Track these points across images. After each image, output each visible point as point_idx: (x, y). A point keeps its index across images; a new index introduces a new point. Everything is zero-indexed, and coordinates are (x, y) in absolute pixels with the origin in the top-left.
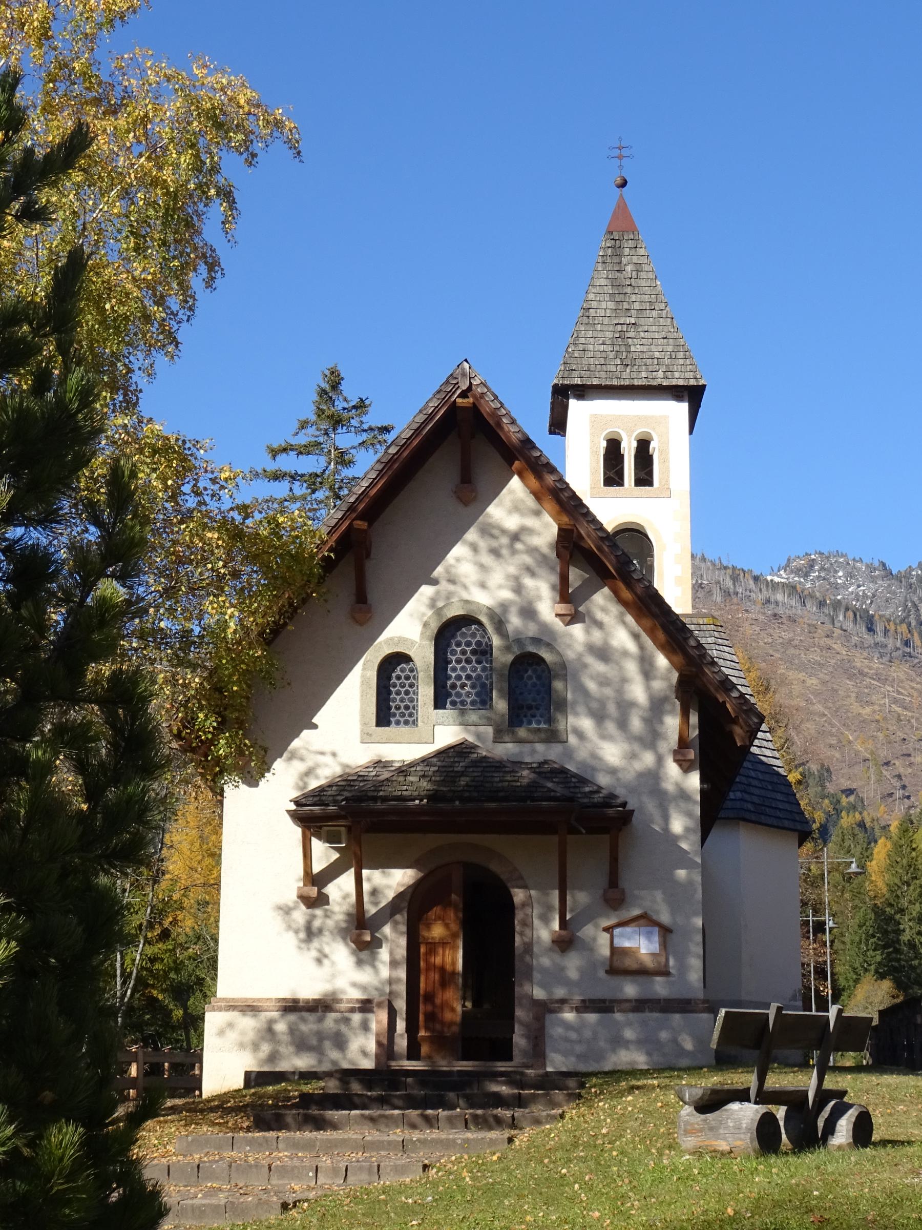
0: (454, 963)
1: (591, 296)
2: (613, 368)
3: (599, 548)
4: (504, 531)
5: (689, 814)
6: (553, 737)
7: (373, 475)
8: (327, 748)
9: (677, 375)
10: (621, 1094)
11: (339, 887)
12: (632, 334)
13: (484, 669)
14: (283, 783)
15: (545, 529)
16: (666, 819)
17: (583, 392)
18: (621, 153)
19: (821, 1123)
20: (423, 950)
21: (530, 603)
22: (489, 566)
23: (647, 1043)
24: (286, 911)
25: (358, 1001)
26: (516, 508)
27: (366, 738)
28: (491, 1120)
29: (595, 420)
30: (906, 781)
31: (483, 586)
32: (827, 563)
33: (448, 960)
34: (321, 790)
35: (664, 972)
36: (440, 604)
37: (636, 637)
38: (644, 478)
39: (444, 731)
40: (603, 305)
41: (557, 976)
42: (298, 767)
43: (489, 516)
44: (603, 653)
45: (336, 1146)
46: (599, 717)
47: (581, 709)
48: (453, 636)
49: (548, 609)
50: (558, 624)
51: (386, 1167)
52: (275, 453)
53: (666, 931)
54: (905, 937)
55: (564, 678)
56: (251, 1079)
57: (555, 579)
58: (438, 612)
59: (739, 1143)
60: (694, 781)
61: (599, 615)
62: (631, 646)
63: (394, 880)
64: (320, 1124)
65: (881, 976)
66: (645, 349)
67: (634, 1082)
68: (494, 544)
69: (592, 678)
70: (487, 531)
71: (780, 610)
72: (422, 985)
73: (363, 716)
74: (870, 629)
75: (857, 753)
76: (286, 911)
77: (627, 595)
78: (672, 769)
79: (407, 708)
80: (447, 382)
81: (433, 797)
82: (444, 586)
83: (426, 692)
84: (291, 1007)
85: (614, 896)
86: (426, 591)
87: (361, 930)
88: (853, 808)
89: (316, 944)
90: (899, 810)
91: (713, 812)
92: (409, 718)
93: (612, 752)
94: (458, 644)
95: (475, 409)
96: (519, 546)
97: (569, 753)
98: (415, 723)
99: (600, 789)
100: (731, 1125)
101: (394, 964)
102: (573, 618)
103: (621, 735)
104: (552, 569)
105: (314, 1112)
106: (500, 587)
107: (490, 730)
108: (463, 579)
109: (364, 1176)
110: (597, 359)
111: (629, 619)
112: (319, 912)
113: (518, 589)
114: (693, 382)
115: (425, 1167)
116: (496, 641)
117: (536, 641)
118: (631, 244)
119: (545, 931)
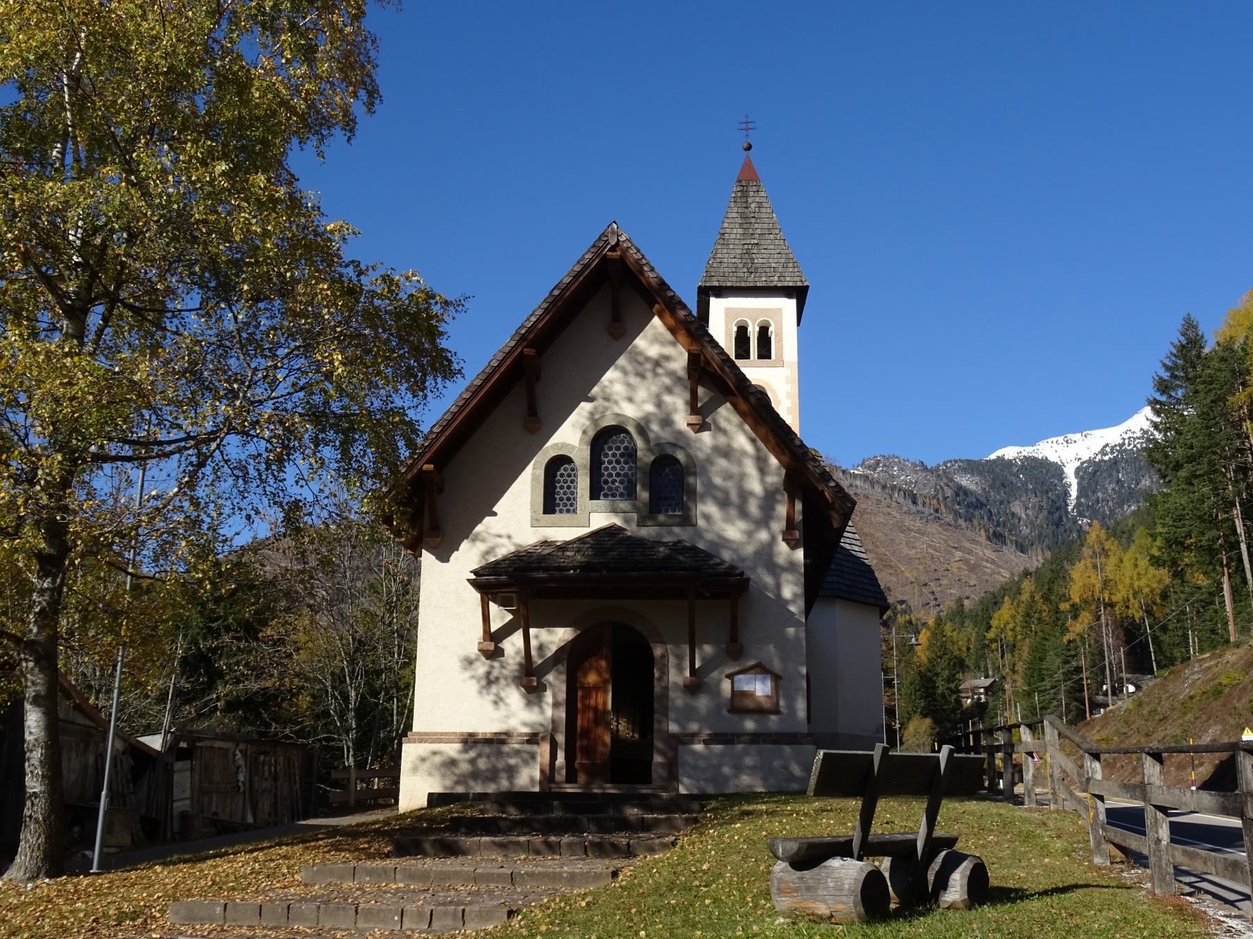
0: (605, 704)
1: (726, 225)
3: (722, 369)
4: (648, 359)
5: (796, 585)
6: (687, 521)
7: (540, 312)
8: (504, 532)
10: (732, 821)
11: (513, 644)
13: (630, 469)
14: (468, 557)
15: (679, 359)
16: (778, 587)
17: (721, 292)
18: (747, 126)
19: (931, 877)
20: (580, 693)
22: (636, 388)
23: (763, 770)
25: (526, 734)
26: (656, 340)
27: (535, 523)
28: (608, 847)
29: (728, 311)
30: (937, 595)
31: (630, 400)
32: (888, 461)
33: (600, 701)
34: (497, 563)
35: (776, 711)
36: (597, 417)
37: (753, 441)
38: (765, 353)
39: (599, 518)
41: (688, 713)
42: (481, 547)
43: (635, 347)
44: (726, 452)
45: (449, 878)
46: (724, 503)
48: (606, 442)
49: (682, 420)
50: (690, 432)
51: (471, 912)
53: (776, 678)
54: (939, 691)
55: (694, 474)
56: (434, 799)
57: (687, 395)
58: (595, 422)
59: (840, 907)
60: (800, 554)
61: (723, 424)
62: (749, 448)
63: (559, 636)
64: (452, 850)
65: (925, 716)
67: (746, 808)
71: (859, 491)
72: (579, 723)
73: (532, 505)
74: (914, 502)
75: (907, 578)
76: (469, 662)
77: (743, 406)
78: (783, 547)
79: (569, 499)
80: (600, 239)
81: (585, 567)
83: (583, 483)
84: (470, 741)
86: (585, 407)
87: (530, 678)
88: (904, 612)
89: (494, 689)
90: (933, 613)
91: (814, 590)
92: (570, 507)
93: (734, 531)
94: (610, 449)
95: (622, 260)
96: (660, 371)
97: (699, 534)
98: (575, 511)
99: (723, 562)
100: (831, 885)
101: (556, 705)
102: (701, 427)
103: (740, 521)
104: (686, 388)
105: (449, 837)
106: (644, 402)
108: (615, 397)
109: (449, 922)
110: (729, 267)
111: (747, 427)
112: (496, 664)
113: (659, 404)
114: (799, 284)
115: (511, 914)
116: (639, 443)
117: (674, 445)
118: (755, 189)
119: (677, 676)
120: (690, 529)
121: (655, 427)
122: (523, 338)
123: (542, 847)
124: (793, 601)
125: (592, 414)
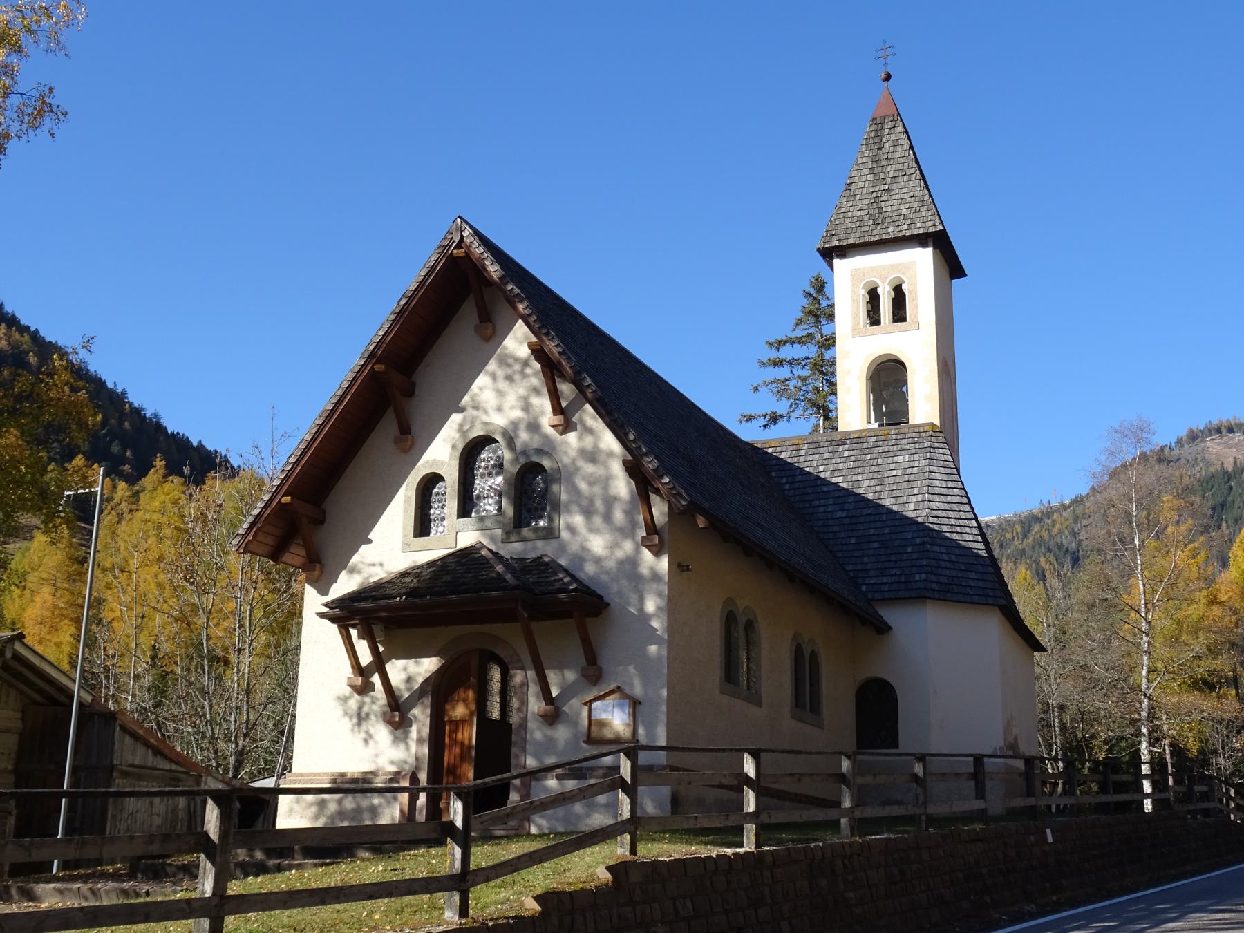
0: (470, 739)
1: (855, 173)
2: (866, 229)
4: (517, 360)
5: (660, 595)
6: (550, 534)
8: (377, 561)
9: (919, 225)
12: (885, 198)
16: (641, 600)
17: (843, 251)
20: (447, 728)
21: (536, 419)
22: (503, 394)
24: (344, 700)
31: (499, 409)
36: (466, 428)
38: (899, 314)
40: (864, 178)
43: (506, 348)
44: (592, 456)
46: (588, 513)
47: (574, 508)
49: (547, 419)
52: (781, 343)
53: (635, 704)
60: (663, 564)
66: (894, 208)
68: (509, 371)
69: (584, 479)
70: (504, 361)
72: (446, 759)
76: (344, 700)
78: (647, 555)
80: (445, 238)
82: (471, 412)
83: (452, 505)
85: (593, 672)
86: (456, 418)
87: (397, 713)
93: (598, 544)
97: (563, 548)
101: (420, 741)
102: (567, 426)
106: (512, 408)
107: (499, 532)
108: (485, 405)
112: (367, 700)
113: (526, 407)
117: (539, 451)
120: (554, 543)
121: (524, 436)
122: (372, 354)
123: (89, 894)
125: (461, 426)
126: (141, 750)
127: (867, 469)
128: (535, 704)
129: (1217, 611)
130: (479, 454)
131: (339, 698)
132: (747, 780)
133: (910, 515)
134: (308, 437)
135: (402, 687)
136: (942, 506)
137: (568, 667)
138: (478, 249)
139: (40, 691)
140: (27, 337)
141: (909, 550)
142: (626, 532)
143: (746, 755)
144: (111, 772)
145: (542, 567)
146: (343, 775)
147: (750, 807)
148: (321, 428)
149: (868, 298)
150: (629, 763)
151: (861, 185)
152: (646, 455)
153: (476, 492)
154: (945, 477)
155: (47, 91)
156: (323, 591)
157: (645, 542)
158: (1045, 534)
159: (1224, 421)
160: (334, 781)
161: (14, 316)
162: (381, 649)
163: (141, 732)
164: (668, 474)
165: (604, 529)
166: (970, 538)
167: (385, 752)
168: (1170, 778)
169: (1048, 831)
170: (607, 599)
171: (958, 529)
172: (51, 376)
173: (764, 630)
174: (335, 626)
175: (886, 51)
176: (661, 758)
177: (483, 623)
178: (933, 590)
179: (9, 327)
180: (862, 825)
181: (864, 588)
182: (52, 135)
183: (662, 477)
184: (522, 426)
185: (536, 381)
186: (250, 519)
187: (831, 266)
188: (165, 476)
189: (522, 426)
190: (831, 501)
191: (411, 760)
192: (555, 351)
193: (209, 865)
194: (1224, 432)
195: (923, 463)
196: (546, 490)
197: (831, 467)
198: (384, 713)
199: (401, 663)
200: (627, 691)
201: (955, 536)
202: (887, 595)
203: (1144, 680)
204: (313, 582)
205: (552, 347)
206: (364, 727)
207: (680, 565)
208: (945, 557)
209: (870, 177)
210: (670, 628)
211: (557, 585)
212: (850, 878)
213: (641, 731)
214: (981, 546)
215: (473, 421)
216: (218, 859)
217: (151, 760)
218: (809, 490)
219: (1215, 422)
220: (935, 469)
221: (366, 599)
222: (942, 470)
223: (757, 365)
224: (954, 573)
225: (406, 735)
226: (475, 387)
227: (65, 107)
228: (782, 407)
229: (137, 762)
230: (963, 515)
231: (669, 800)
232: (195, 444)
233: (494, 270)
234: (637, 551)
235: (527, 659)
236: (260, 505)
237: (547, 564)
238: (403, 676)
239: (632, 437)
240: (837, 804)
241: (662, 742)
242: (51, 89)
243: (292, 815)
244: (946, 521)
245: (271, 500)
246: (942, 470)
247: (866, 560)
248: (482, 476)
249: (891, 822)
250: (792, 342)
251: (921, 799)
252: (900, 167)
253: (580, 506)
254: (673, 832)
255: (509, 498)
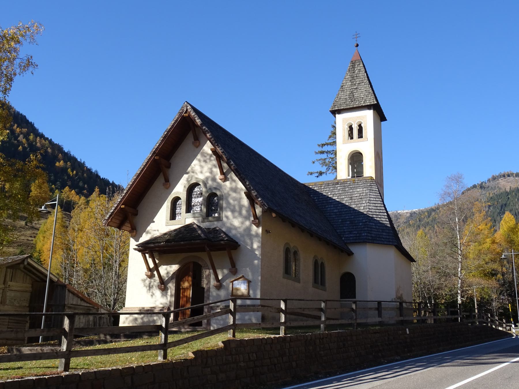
0: (190, 295)
1: (344, 82)
4: (208, 154)
5: (259, 242)
6: (219, 219)
8: (156, 229)
16: (252, 244)
17: (339, 111)
22: (202, 167)
24: (144, 281)
31: (201, 172)
38: (360, 135)
43: (204, 150)
44: (235, 190)
46: (233, 211)
47: (228, 209)
52: (323, 145)
53: (249, 282)
60: (260, 230)
68: (205, 159)
69: (232, 198)
76: (144, 281)
78: (254, 227)
82: (191, 174)
83: (184, 208)
86: (185, 176)
87: (163, 285)
93: (236, 222)
97: (224, 224)
101: (171, 296)
102: (225, 179)
106: (206, 172)
107: (200, 219)
112: (152, 280)
113: (211, 172)
121: (210, 182)
122: (154, 153)
124: (257, 249)
125: (188, 179)
126: (76, 299)
127: (346, 194)
128: (213, 282)
129: (496, 246)
130: (194, 189)
131: (142, 280)
132: (282, 311)
133: (362, 211)
134: (131, 183)
135: (165, 276)
136: (374, 208)
137: (225, 268)
138: (193, 114)
139: (38, 277)
140: (47, 142)
141: (361, 224)
142: (247, 218)
143: (282, 301)
144: (65, 307)
145: (215, 231)
146: (143, 308)
147: (283, 320)
148: (135, 180)
149: (349, 129)
150: (233, 304)
151: (347, 86)
152: (253, 190)
153: (193, 204)
154: (375, 197)
155: (30, 58)
156: (137, 240)
157: (253, 222)
158: (436, 216)
159: (506, 172)
160: (140, 310)
161: (42, 134)
162: (157, 262)
163: (76, 292)
164: (260, 197)
165: (237, 218)
166: (384, 220)
167: (159, 300)
168: (476, 310)
169: (407, 330)
170: (239, 243)
171: (380, 216)
172: (29, 162)
173: (302, 255)
174: (140, 253)
175: (357, 36)
176: (258, 302)
177: (193, 252)
178: (369, 239)
179: (41, 138)
180: (327, 327)
181: (343, 239)
182: (32, 73)
183: (258, 198)
184: (210, 179)
185: (215, 162)
186: (109, 214)
187: (335, 117)
188: (99, 195)
189: (210, 179)
190: (332, 206)
191: (168, 303)
192: (220, 151)
193: (65, 340)
194: (506, 176)
195: (367, 191)
196: (218, 202)
197: (333, 193)
198: (158, 286)
199: (164, 267)
200: (246, 277)
201: (378, 219)
202: (352, 241)
203: (459, 273)
204: (133, 237)
205: (219, 150)
206: (151, 291)
207: (266, 231)
208: (374, 227)
209: (350, 83)
210: (262, 254)
211: (220, 238)
212: (322, 346)
213: (251, 292)
214: (388, 223)
215: (192, 177)
216: (68, 338)
217: (80, 302)
218: (324, 202)
219: (503, 173)
220: (372, 194)
221: (151, 243)
222: (374, 194)
223: (314, 153)
224: (377, 233)
225: (167, 293)
226: (192, 164)
227: (37, 63)
228: (324, 169)
229: (74, 303)
230: (381, 211)
231: (260, 317)
232: (111, 182)
233: (198, 121)
234: (251, 225)
235: (210, 267)
236: (113, 208)
237: (217, 230)
238: (166, 272)
239: (247, 183)
240: (319, 318)
241: (259, 296)
242: (31, 57)
243: (124, 321)
244: (375, 213)
245: (117, 207)
246: (374, 194)
247: (344, 228)
248: (195, 198)
249: (341, 326)
250: (327, 144)
251: (355, 317)
252: (361, 79)
253: (230, 209)
254: (258, 329)
255: (204, 205)
